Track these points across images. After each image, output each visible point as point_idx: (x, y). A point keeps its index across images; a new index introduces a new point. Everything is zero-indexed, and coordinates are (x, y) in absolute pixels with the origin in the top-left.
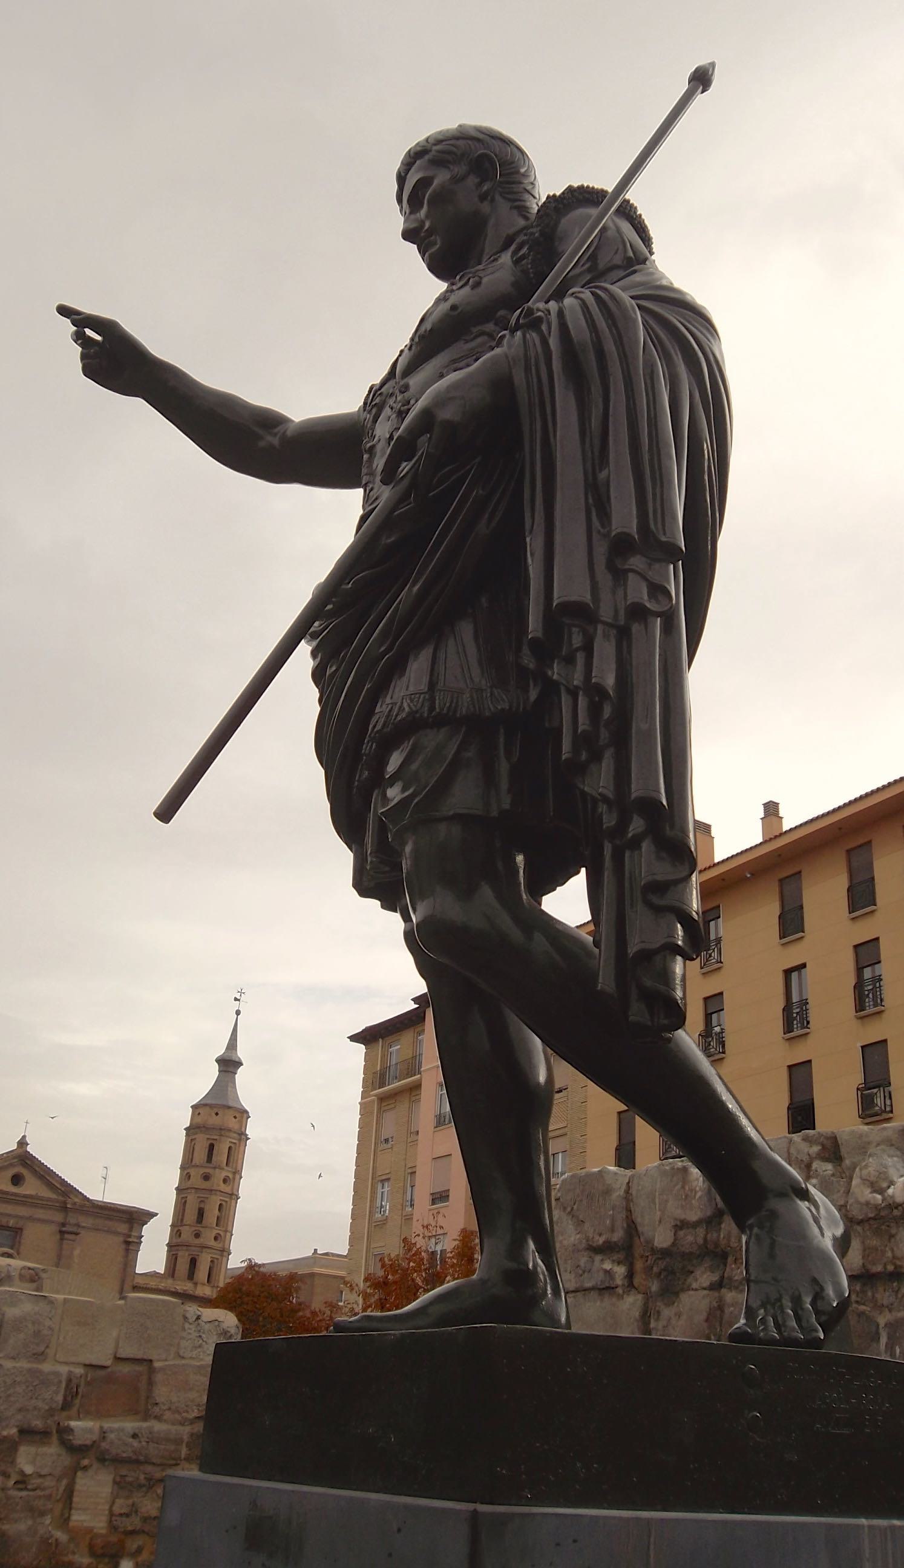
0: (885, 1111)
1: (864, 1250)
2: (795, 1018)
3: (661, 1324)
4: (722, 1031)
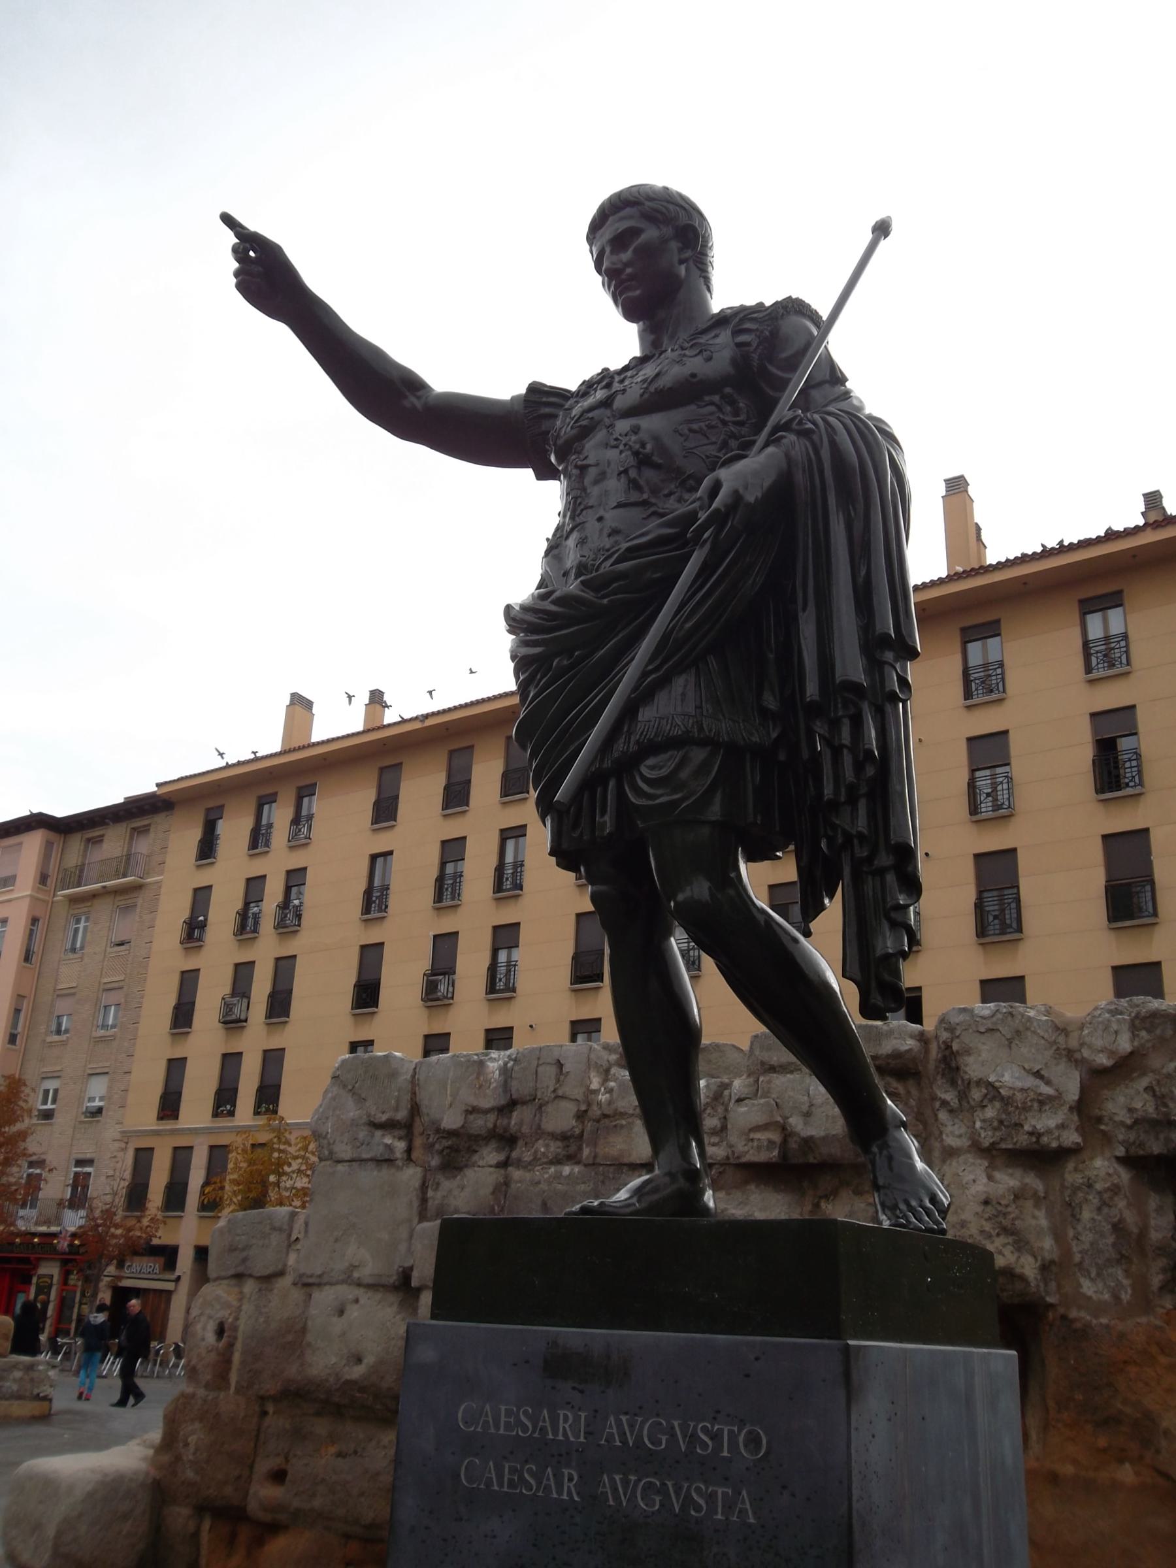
2: (374, 901)
3: (439, 1194)
4: (301, 904)
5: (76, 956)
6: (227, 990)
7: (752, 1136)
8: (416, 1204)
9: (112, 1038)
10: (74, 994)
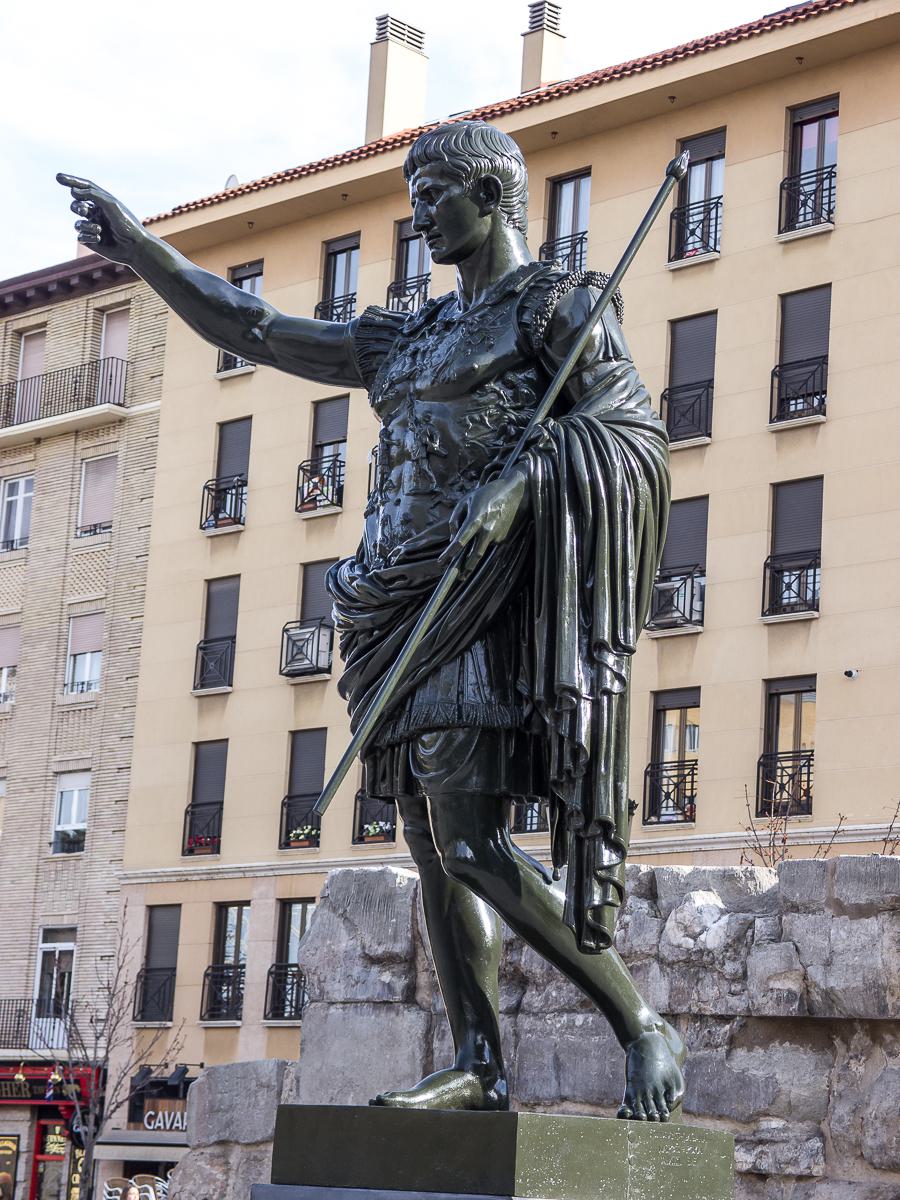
0: (689, 621)
1: (672, 990)
5: (14, 555)
6: (293, 612)
7: (773, 984)
8: (419, 1055)
9: (92, 707)
10: (17, 626)
